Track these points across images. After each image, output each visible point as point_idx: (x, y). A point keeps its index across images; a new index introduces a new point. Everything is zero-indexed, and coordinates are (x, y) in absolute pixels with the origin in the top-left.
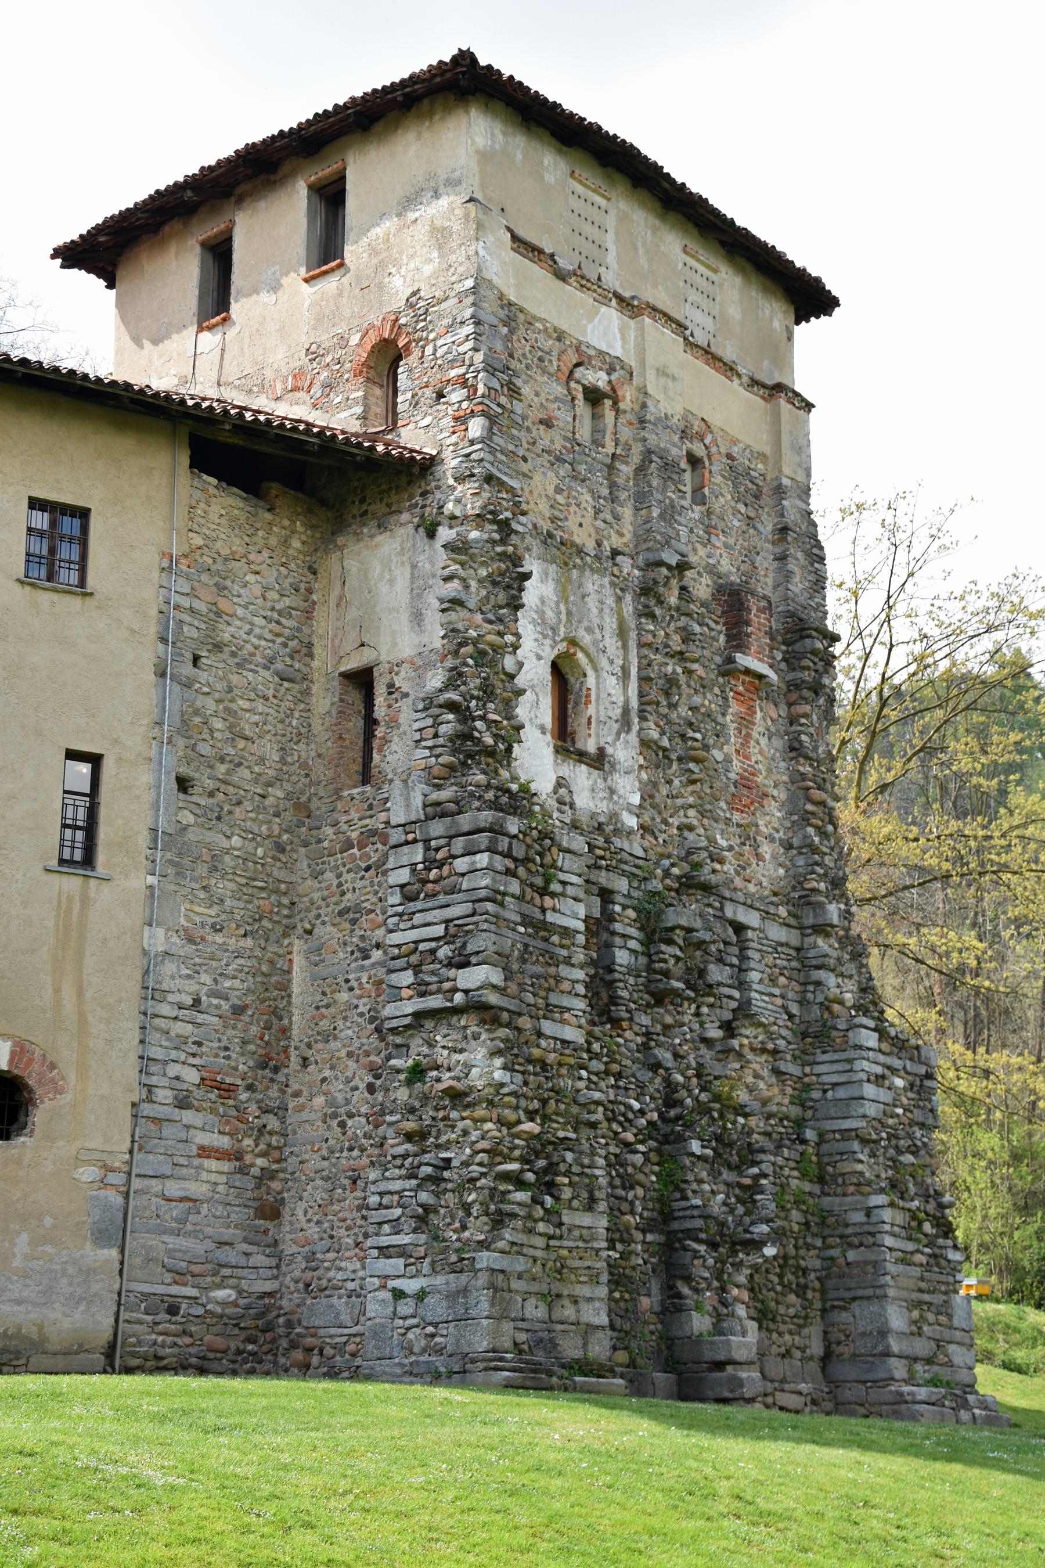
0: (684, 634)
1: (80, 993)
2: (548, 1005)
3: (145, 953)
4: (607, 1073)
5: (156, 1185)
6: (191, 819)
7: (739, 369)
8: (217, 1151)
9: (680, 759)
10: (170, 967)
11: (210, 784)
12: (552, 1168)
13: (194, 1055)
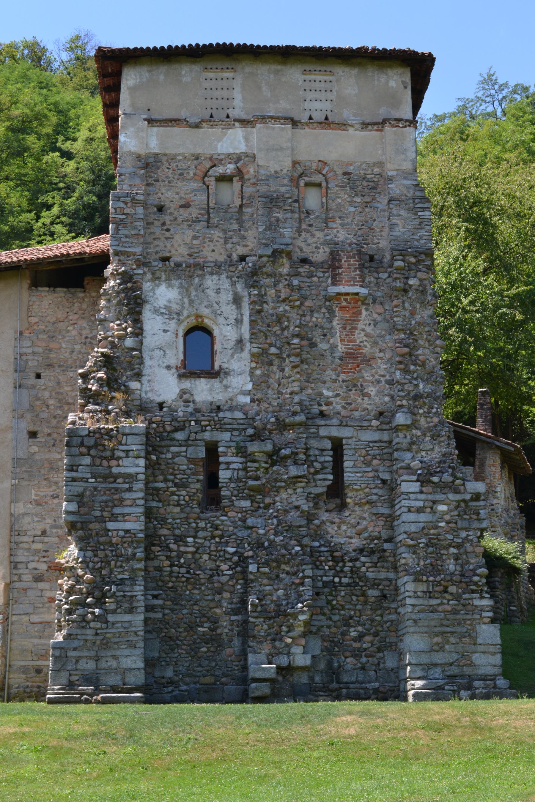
2: (112, 514)
3: (12, 515)
4: (213, 537)
5: (25, 618)
7: (349, 122)
10: (27, 519)
11: (47, 431)
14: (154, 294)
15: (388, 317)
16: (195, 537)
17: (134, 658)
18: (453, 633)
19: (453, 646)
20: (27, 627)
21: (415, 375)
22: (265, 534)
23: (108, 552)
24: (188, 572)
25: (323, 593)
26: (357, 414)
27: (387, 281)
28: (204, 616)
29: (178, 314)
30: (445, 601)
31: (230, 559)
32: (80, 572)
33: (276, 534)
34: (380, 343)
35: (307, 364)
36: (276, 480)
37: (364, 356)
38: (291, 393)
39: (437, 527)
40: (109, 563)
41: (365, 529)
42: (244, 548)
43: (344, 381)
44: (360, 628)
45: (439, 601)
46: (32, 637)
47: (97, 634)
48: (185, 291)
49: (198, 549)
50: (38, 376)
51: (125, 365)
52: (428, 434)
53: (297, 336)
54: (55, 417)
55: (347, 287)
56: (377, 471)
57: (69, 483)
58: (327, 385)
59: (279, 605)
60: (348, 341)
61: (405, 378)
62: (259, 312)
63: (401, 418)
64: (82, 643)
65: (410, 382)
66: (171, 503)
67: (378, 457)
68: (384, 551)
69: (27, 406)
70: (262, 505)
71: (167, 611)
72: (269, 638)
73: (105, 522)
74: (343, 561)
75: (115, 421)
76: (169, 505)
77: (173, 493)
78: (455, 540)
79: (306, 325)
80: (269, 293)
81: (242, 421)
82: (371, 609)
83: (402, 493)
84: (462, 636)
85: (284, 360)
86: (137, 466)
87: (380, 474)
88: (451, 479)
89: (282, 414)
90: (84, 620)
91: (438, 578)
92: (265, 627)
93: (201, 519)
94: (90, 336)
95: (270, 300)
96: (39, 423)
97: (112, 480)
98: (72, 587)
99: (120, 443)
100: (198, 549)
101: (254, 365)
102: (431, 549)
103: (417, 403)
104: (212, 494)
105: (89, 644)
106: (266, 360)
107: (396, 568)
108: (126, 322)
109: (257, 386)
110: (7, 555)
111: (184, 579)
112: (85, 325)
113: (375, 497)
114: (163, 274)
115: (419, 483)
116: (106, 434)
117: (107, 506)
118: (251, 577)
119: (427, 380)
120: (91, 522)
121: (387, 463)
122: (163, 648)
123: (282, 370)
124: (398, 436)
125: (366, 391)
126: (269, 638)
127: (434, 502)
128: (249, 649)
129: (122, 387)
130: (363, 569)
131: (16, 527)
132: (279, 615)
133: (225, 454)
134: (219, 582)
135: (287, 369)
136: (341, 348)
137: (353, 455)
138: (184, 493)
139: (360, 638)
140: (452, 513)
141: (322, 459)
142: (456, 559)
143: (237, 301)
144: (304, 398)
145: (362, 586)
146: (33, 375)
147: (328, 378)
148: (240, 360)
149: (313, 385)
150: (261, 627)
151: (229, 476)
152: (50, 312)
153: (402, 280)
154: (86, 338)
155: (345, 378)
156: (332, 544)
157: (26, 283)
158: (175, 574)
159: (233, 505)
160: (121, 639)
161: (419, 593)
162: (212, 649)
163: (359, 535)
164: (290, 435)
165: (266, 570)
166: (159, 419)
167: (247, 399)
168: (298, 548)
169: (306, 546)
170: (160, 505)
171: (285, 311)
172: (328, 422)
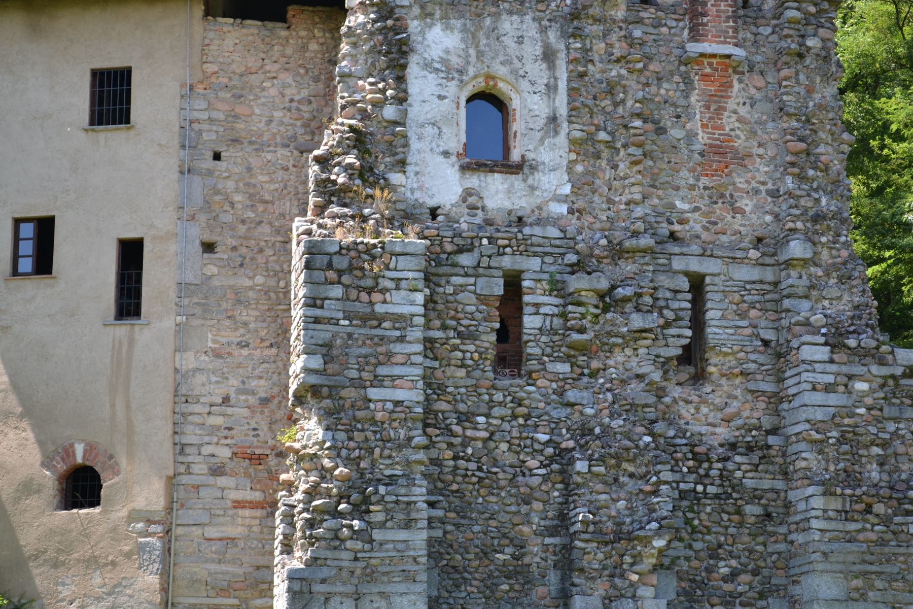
0: (629, 41)
1: (128, 407)
2: (376, 376)
4: (515, 417)
5: (197, 531)
6: (215, 270)
8: (251, 502)
9: (625, 146)
10: (200, 378)
12: (366, 500)
13: (226, 438)
14: (424, 39)
15: (771, 95)
16: (487, 416)
17: (413, 597)
18: (879, 574)
19: (879, 593)
20: (199, 544)
21: (815, 185)
22: (595, 416)
23: (369, 434)
24: (480, 469)
25: (680, 507)
26: (724, 239)
27: (771, 39)
28: (505, 536)
29: (461, 72)
30: (868, 526)
31: (541, 452)
32: (327, 463)
33: (611, 416)
34: (759, 132)
35: (652, 159)
36: (609, 334)
37: (735, 151)
38: (628, 203)
39: (852, 415)
40: (371, 451)
41: (738, 414)
42: (561, 435)
43: (705, 188)
44: (734, 563)
45: (859, 526)
46: (207, 561)
47: (356, 559)
48: (470, 36)
49: (492, 434)
50: (217, 157)
51: (383, 146)
52: (834, 275)
53: (638, 115)
54: (243, 222)
55: (714, 45)
56: (755, 327)
57: (311, 326)
58: (681, 193)
59: (620, 524)
60: (714, 128)
61: (799, 188)
62: (582, 75)
63: (797, 249)
64: (334, 572)
65: (809, 195)
66: (453, 362)
67: (757, 305)
68: (769, 447)
69: (199, 201)
70: (586, 371)
71: (449, 528)
72: (606, 572)
73: (365, 388)
74: (708, 460)
75: (377, 234)
76: (449, 365)
77: (455, 348)
78: (880, 435)
79: (652, 100)
80: (595, 48)
81: (558, 242)
82: (749, 534)
83: (803, 362)
84: (892, 578)
85: (617, 151)
86: (413, 303)
87: (761, 332)
88: (874, 344)
89: (617, 234)
90: (337, 537)
91: (858, 492)
92: (601, 556)
93: (496, 389)
94: (297, 98)
95: (596, 58)
96: (219, 230)
97: (375, 323)
98: (316, 486)
99: (387, 268)
100: (492, 434)
101: (573, 156)
102: (845, 448)
103: (818, 227)
104: (509, 352)
105: (345, 574)
106: (591, 149)
107: (786, 473)
108: (384, 80)
109: (577, 188)
110: (170, 432)
111: (475, 479)
112: (290, 80)
113: (753, 366)
114: (437, 8)
115: (828, 348)
116: (365, 253)
117: (368, 363)
118: (579, 480)
119: (831, 192)
120: (344, 387)
121: (772, 316)
122: (444, 583)
123: (615, 167)
124: (789, 276)
125: (738, 205)
126: (606, 572)
127: (850, 377)
128: (574, 589)
129: (382, 181)
130: (738, 474)
131: (183, 390)
132: (620, 539)
133: (532, 291)
134: (527, 485)
135: (622, 166)
136: (702, 138)
137: (721, 300)
138: (472, 348)
139: (733, 576)
140: (876, 395)
141: (675, 305)
142: (881, 464)
143: (548, 56)
144: (648, 211)
145: (736, 500)
146: (210, 155)
147: (683, 183)
148: (553, 147)
149: (660, 192)
150: (593, 555)
151: (538, 325)
152: (236, 57)
153: (796, 39)
154: (292, 101)
155: (707, 184)
156: (688, 434)
157: (199, 10)
158: (463, 472)
159: (545, 369)
160: (393, 568)
161: (831, 513)
162: (517, 587)
163: (729, 421)
164: (628, 268)
165: (602, 469)
166: (434, 232)
167: (563, 209)
168: (648, 439)
169: (660, 436)
170: (436, 364)
171: (620, 76)
172: (685, 250)
